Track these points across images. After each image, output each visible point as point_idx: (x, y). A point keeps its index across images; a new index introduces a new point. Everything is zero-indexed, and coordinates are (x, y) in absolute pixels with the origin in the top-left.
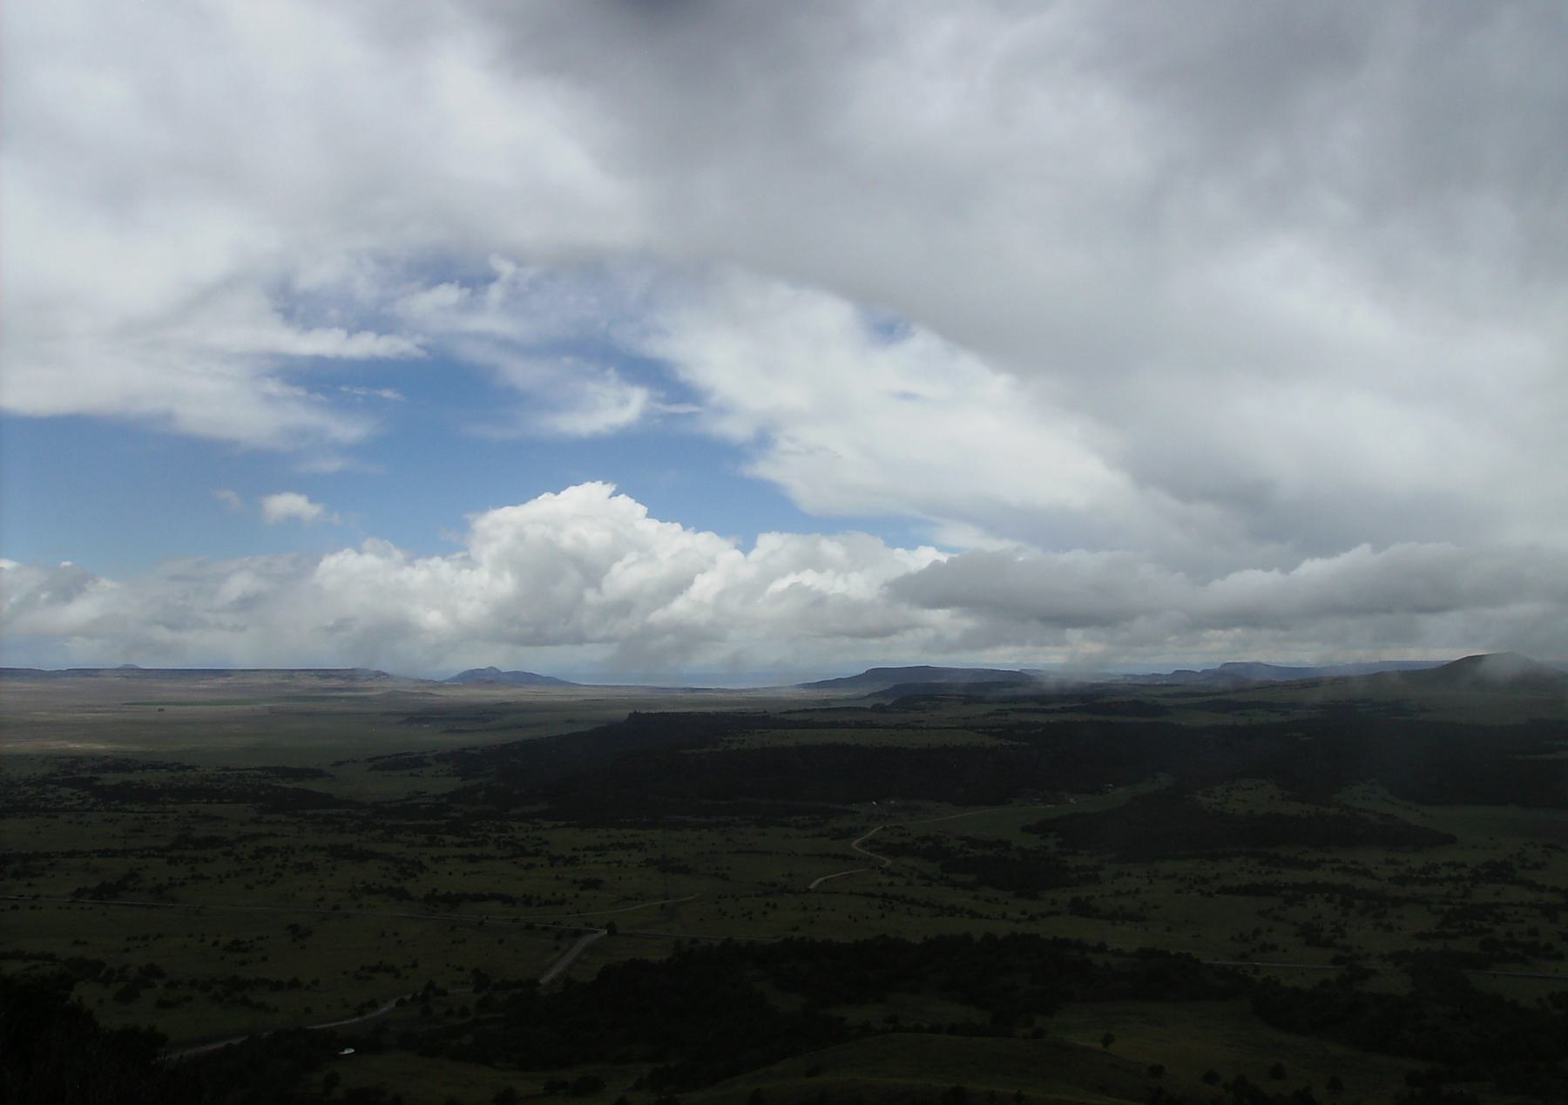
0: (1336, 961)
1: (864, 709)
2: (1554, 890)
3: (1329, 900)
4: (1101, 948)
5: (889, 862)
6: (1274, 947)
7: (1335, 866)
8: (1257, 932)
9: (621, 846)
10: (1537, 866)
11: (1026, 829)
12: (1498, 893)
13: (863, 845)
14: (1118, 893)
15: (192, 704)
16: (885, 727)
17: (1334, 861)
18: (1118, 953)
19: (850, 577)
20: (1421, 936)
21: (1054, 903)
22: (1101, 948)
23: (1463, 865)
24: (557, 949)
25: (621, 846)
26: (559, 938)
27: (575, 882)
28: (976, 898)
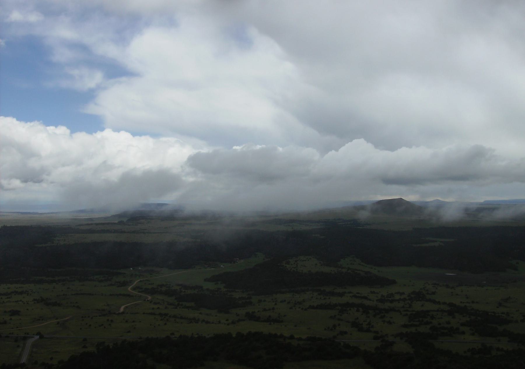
0: (375, 338)
1: (114, 223)
2: (444, 303)
3: (358, 311)
4: (292, 337)
5: (150, 298)
6: (346, 333)
7: (351, 295)
8: (334, 326)
9: (16, 293)
10: (434, 293)
11: (206, 280)
12: (422, 306)
13: (134, 289)
14: (265, 310)
15: (108, 231)
16: (128, 232)
17: (350, 293)
18: (300, 339)
19: (173, 155)
20: (405, 326)
21: (238, 315)
22: (292, 337)
23: (403, 293)
24: (18, 346)
25: (16, 293)
26: (16, 341)
27: (5, 312)
28: (201, 313)
